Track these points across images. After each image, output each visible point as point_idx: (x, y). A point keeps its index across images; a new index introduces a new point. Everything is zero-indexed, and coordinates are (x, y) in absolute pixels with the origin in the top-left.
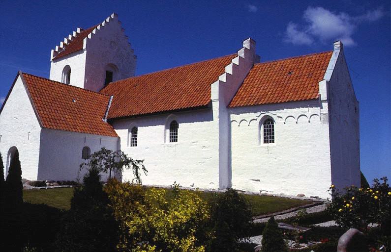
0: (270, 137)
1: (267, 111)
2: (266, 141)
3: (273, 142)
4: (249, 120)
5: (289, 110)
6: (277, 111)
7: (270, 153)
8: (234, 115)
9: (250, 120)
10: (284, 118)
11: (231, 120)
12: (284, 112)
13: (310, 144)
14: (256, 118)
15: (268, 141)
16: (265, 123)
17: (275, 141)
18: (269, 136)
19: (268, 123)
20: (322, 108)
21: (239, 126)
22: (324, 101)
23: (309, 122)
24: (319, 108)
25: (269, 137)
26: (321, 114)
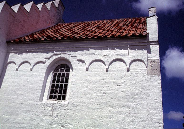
0: (60, 91)
1: (63, 51)
2: (51, 97)
3: (64, 99)
4: (33, 62)
5: (98, 51)
6: (79, 52)
7: (54, 115)
8: (15, 55)
9: (110, 60)
10: (87, 63)
11: (9, 61)
12: (89, 55)
13: (127, 106)
14: (44, 60)
15: (55, 96)
16: (56, 70)
17: (67, 98)
18: (58, 89)
19: (62, 70)
20: (149, 52)
21: (17, 70)
22: (154, 43)
23: (107, 70)
24: (146, 51)
25: (58, 91)
26: (148, 60)
